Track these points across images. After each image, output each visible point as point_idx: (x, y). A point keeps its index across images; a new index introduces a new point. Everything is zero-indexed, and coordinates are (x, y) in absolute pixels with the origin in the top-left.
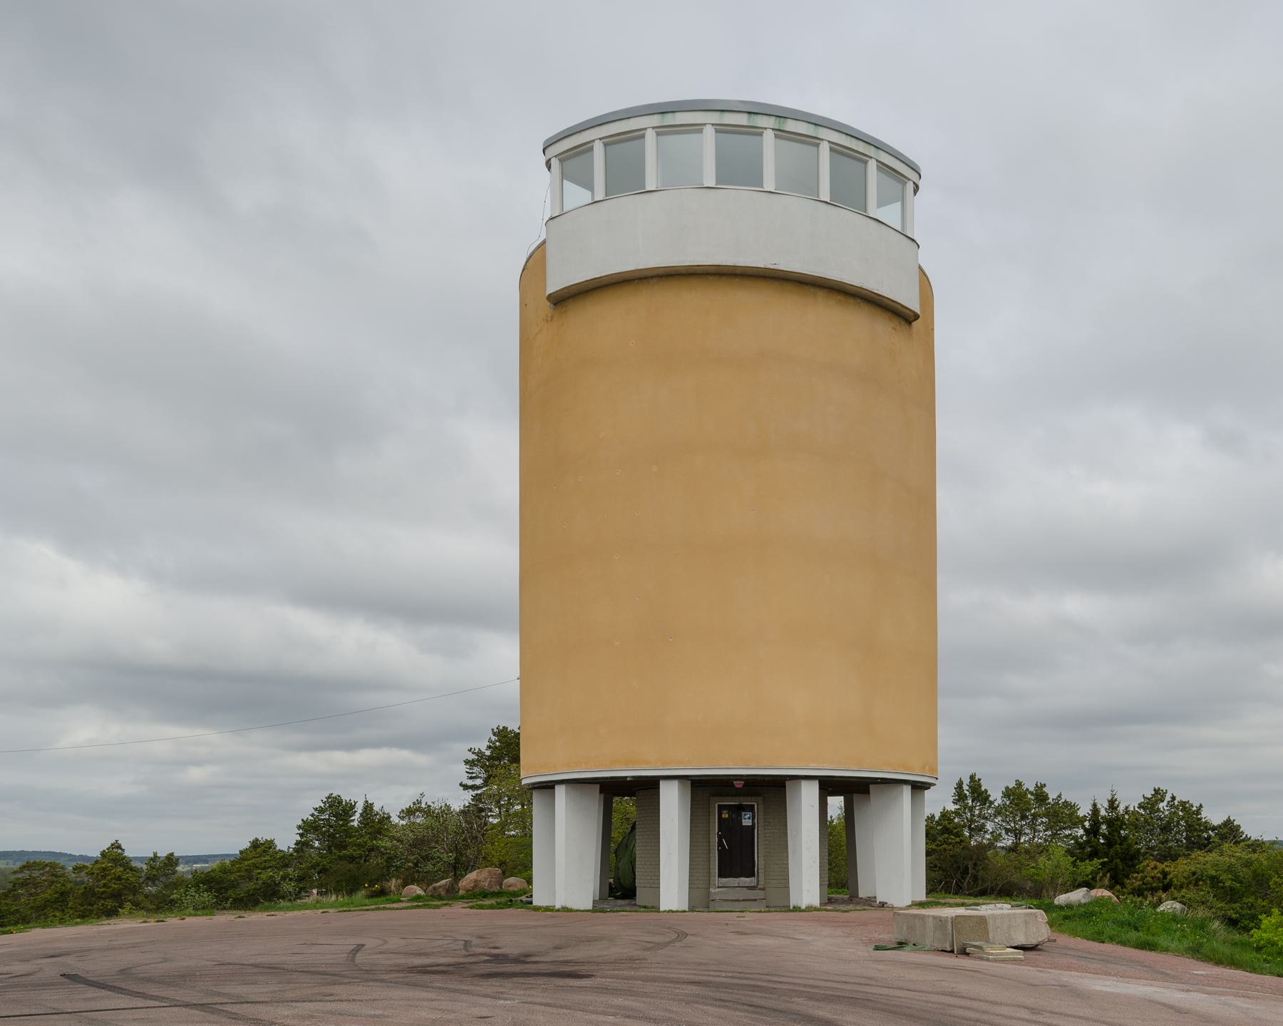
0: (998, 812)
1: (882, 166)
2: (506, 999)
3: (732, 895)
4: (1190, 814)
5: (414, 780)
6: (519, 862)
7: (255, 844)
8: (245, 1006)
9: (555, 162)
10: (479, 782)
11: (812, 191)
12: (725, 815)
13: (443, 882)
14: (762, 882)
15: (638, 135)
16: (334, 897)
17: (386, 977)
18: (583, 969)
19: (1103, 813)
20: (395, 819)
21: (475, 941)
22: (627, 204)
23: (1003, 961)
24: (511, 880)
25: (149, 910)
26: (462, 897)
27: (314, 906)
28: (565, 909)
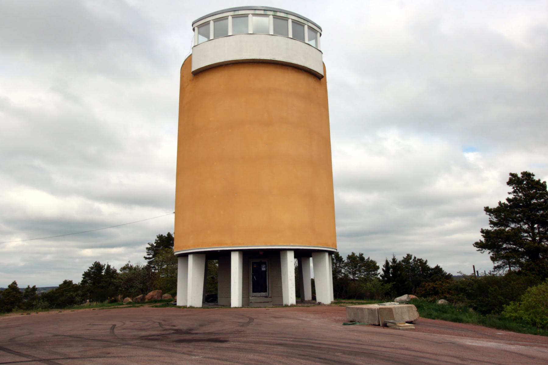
0: (347, 265)
1: (310, 28)
2: (195, 355)
3: (259, 300)
4: (422, 264)
5: (127, 256)
6: (171, 287)
7: (65, 282)
8: (69, 360)
9: (196, 29)
10: (151, 256)
11: (286, 35)
12: (255, 266)
13: (140, 296)
14: (270, 295)
15: (226, 18)
16: (95, 303)
17: (132, 342)
18: (221, 337)
19: (390, 264)
20: (118, 271)
21: (163, 323)
22: (222, 40)
23: (407, 330)
24: (166, 295)
25: (24, 309)
26: (147, 303)
27: (89, 307)
28: (191, 307)
